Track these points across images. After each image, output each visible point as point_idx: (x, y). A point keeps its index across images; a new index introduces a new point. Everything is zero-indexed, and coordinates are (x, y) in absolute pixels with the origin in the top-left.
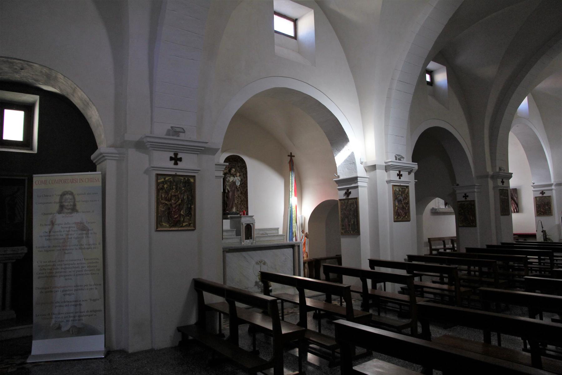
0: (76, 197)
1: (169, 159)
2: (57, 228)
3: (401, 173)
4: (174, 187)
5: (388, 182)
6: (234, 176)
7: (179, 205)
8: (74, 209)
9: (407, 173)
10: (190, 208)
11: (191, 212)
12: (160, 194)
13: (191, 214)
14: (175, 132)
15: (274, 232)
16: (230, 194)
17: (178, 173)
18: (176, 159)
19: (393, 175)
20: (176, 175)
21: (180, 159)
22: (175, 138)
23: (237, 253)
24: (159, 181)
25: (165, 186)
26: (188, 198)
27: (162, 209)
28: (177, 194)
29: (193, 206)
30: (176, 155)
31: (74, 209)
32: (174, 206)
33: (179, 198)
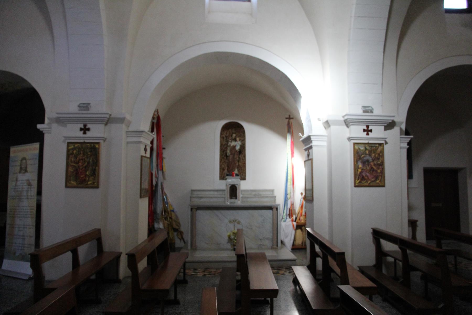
0: (28, 161)
1: (79, 129)
2: (18, 183)
3: (88, 126)
4: (82, 152)
5: (349, 139)
6: (235, 140)
7: (85, 167)
8: (26, 171)
9: (383, 127)
10: (95, 170)
11: (95, 173)
12: (70, 158)
13: (95, 174)
14: (85, 107)
15: (269, 193)
16: (231, 157)
17: (86, 141)
18: (85, 130)
19: (357, 132)
20: (84, 143)
21: (89, 129)
22: (87, 112)
23: (210, 211)
24: (70, 148)
25: (75, 152)
26: (93, 161)
27: (71, 170)
28: (84, 158)
29: (97, 168)
30: (85, 126)
31: (26, 171)
32: (81, 168)
33: (85, 161)
